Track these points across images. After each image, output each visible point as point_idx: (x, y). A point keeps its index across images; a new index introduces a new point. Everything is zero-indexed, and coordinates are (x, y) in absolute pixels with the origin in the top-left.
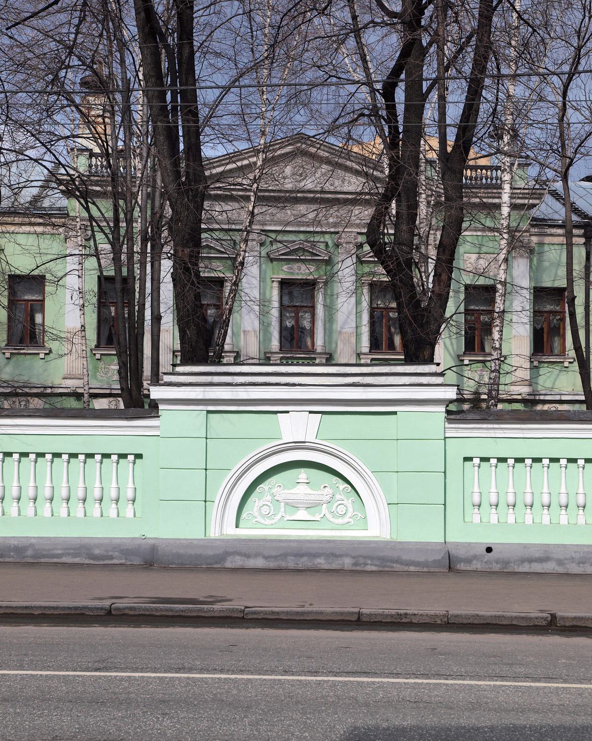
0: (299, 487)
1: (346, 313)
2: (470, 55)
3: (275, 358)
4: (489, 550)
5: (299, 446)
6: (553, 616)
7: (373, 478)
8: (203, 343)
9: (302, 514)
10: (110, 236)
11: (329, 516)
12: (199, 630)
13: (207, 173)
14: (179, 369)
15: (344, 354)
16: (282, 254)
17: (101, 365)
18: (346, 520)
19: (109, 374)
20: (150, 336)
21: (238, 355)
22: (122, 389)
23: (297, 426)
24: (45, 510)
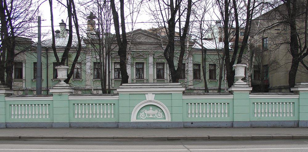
0: (151, 111)
1: (151, 72)
2: (186, 12)
3: (135, 81)
4: (192, 123)
5: (151, 101)
6: (209, 137)
7: (167, 108)
8: (125, 79)
9: (151, 116)
10: (99, 53)
11: (157, 117)
12: (229, 136)
13: (185, 44)
14: (123, 85)
15: (151, 80)
16: (115, 56)
17: (95, 82)
18: (161, 117)
19: (99, 85)
20: (14, 73)
21: (147, 80)
22: (102, 88)
23: (150, 97)
24: (16, 117)
